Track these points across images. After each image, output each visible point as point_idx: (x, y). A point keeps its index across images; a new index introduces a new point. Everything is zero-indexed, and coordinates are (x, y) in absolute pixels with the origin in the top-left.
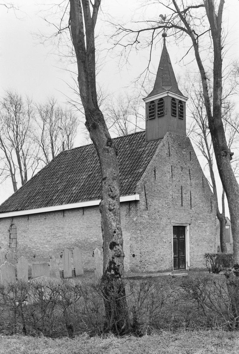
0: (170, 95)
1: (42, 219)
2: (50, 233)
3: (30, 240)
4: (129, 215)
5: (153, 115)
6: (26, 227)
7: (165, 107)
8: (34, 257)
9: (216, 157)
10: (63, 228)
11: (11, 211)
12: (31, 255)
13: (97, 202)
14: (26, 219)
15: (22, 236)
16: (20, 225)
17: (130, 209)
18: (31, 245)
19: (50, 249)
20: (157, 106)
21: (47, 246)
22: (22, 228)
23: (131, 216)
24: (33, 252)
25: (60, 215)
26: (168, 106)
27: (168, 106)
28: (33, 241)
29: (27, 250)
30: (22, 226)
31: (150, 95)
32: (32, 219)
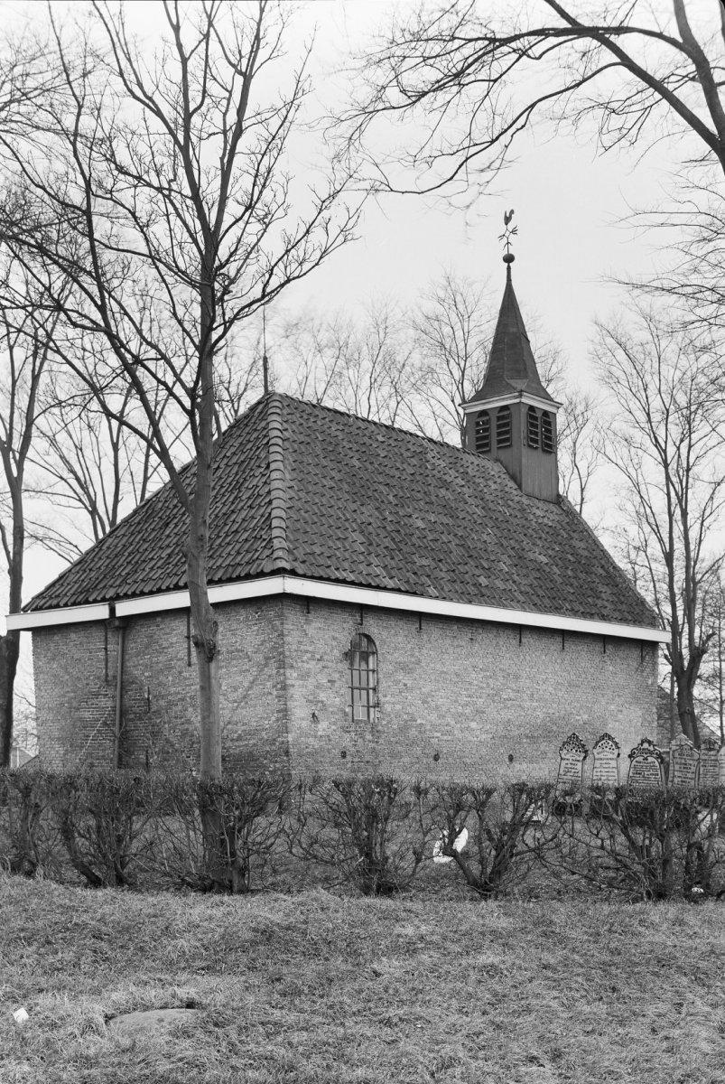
0: (523, 400)
1: (506, 641)
2: (485, 686)
3: (424, 702)
4: (642, 671)
5: (486, 445)
6: (412, 655)
7: (514, 430)
8: (436, 758)
9: (21, 584)
10: (517, 677)
11: (164, 587)
12: (427, 751)
13: (181, 599)
14: (598, 647)
15: (397, 682)
16: (393, 643)
17: (643, 658)
18: (426, 718)
19: (484, 736)
20: (494, 423)
21: (473, 725)
22: (398, 656)
23: (645, 674)
24: (433, 741)
25: (554, 645)
26: (520, 427)
27: (520, 427)
28: (433, 704)
29: (413, 732)
30: (396, 649)
31: (479, 396)
32: (434, 631)
